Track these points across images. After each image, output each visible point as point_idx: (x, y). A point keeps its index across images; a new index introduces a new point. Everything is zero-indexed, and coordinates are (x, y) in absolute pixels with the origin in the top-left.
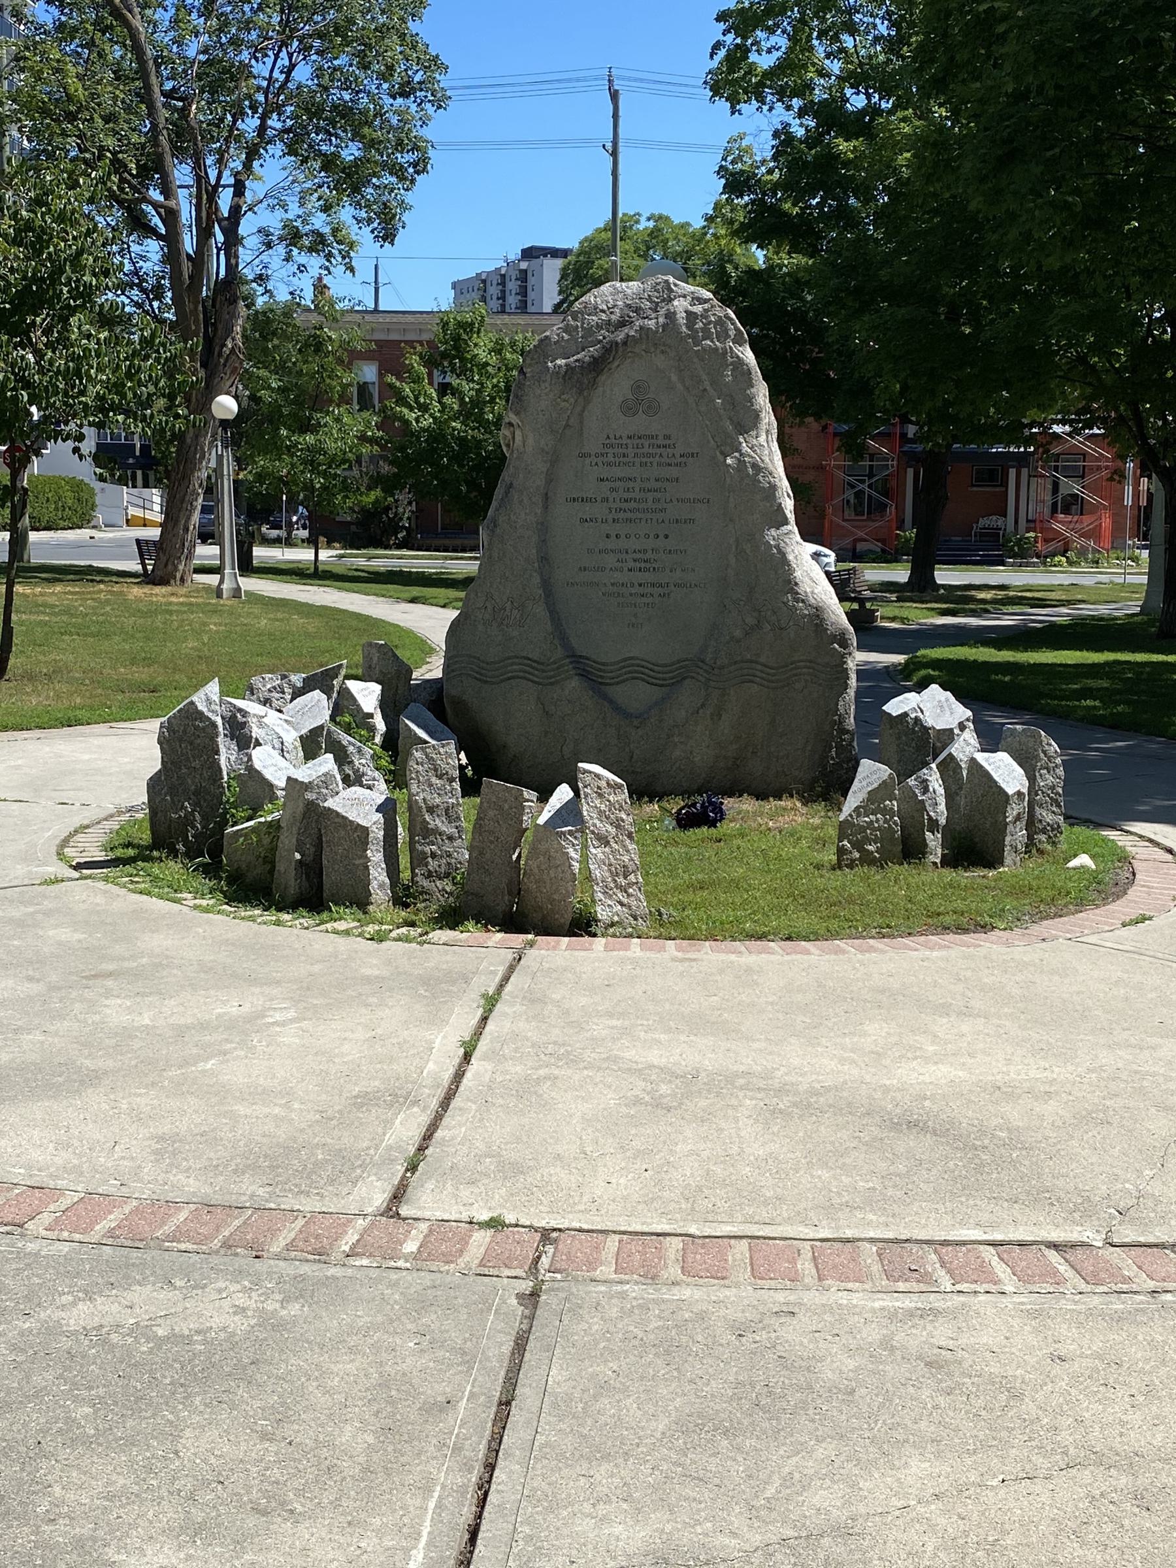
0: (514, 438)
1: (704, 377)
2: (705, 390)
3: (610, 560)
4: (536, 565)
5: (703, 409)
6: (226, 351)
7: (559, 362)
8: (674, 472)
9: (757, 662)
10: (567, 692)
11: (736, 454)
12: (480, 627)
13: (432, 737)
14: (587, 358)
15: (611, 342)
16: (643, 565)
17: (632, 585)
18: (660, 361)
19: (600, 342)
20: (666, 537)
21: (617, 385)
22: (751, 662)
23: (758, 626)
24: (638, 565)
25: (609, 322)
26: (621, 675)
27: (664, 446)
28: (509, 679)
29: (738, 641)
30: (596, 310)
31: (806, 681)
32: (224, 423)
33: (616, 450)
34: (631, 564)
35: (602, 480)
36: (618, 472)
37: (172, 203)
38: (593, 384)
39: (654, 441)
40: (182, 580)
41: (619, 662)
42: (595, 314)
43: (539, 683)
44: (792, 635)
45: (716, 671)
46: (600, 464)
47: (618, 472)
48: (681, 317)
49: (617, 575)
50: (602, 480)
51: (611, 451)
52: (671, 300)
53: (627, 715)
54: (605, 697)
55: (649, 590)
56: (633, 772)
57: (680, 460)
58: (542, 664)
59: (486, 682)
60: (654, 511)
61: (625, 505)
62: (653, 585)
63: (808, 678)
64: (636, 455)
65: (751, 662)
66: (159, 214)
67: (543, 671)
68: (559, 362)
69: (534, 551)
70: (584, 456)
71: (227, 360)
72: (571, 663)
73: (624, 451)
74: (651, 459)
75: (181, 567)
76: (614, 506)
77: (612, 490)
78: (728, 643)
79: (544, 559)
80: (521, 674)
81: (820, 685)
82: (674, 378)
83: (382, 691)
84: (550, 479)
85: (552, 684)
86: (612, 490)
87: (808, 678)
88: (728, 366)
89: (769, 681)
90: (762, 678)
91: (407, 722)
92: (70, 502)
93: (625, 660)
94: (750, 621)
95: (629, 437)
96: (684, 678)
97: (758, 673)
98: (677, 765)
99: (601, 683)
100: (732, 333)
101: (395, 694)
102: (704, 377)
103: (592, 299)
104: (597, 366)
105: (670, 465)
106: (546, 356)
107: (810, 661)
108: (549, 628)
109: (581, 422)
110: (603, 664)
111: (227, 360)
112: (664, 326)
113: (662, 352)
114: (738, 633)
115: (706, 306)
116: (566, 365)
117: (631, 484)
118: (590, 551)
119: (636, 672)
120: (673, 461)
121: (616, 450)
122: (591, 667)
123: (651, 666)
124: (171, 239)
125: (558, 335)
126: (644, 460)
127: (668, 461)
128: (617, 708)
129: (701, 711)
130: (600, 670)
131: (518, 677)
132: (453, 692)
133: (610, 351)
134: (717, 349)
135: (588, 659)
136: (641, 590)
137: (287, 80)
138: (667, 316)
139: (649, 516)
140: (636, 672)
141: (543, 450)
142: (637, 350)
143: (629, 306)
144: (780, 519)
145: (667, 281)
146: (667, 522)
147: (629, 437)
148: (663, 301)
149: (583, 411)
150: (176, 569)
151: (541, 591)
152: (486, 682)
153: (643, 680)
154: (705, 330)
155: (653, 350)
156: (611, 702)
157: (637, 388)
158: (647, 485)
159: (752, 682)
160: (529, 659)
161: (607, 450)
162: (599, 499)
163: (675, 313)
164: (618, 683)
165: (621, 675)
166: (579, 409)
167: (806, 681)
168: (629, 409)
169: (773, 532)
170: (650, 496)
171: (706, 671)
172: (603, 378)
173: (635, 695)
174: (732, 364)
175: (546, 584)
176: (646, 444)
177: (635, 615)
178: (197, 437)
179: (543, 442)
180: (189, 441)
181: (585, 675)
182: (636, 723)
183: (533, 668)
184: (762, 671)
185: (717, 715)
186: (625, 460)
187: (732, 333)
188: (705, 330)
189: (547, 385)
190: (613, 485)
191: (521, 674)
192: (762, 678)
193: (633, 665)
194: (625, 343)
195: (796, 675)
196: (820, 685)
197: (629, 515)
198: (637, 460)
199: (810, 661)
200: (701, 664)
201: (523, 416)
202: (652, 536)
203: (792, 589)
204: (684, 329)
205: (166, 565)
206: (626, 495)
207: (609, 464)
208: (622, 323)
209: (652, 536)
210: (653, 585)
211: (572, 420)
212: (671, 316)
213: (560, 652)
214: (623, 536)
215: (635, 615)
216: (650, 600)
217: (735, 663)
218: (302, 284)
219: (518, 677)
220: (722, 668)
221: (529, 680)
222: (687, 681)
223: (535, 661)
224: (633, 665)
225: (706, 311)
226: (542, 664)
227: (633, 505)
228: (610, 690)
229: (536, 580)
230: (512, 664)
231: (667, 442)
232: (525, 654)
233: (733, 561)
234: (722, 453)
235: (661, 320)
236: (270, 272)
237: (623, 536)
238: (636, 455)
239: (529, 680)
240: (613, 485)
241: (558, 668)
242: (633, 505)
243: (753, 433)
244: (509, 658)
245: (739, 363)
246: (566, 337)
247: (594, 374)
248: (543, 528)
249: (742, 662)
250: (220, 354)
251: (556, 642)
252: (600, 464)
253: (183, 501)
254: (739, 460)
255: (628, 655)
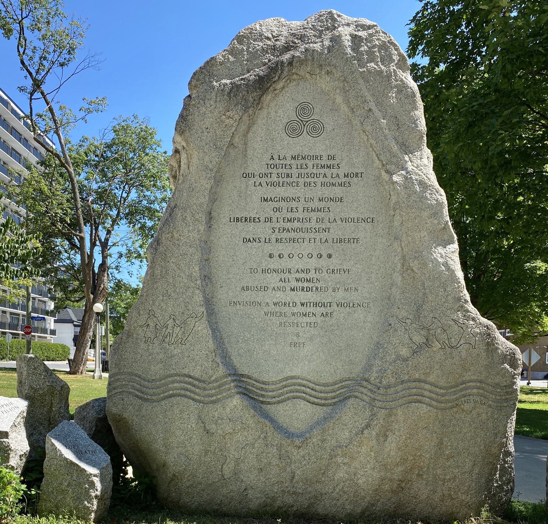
0: (180, 166)
1: (369, 98)
2: (370, 110)
3: (273, 280)
4: (199, 282)
5: (368, 128)
6: (101, 289)
7: (224, 81)
8: (337, 191)
9: (425, 382)
10: (228, 410)
11: (404, 172)
12: (143, 345)
13: (80, 459)
14: (253, 77)
15: (277, 63)
16: (306, 285)
17: (295, 304)
18: (324, 83)
19: (264, 64)
20: (330, 256)
21: (281, 106)
22: (419, 381)
23: (427, 343)
24: (300, 284)
25: (274, 48)
26: (282, 394)
27: (329, 167)
28: (171, 396)
29: (406, 360)
30: (261, 37)
31: (475, 402)
32: (98, 314)
33: (280, 171)
34: (294, 284)
35: (266, 200)
36: (281, 192)
37: (82, 235)
38: (258, 101)
39: (316, 162)
40: (82, 373)
41: (281, 381)
42: (261, 40)
43: (200, 402)
44: (464, 354)
45: (382, 391)
46: (264, 184)
47: (281, 192)
48: (347, 41)
49: (279, 294)
50: (266, 200)
51: (275, 171)
52: (335, 28)
53: (289, 435)
54: (266, 416)
55: (312, 309)
56: (294, 493)
57: (344, 180)
58: (204, 382)
59: (147, 400)
60: (317, 231)
61: (289, 225)
62: (316, 304)
63: (478, 399)
64: (300, 175)
65: (419, 381)
66: (77, 238)
67: (205, 389)
68: (224, 81)
69: (197, 268)
70: (246, 176)
71: (101, 292)
72: (234, 381)
73: (289, 171)
74: (316, 179)
75: (81, 368)
76: (278, 225)
77: (278, 210)
78: (395, 362)
79: (207, 278)
80: (183, 392)
81: (490, 406)
82: (339, 99)
83: (29, 407)
84: (214, 198)
85: (213, 402)
86: (278, 210)
87: (478, 399)
88: (392, 88)
89: (437, 401)
90: (430, 398)
91: (54, 441)
92: (61, 352)
93: (287, 379)
94: (418, 339)
95: (293, 158)
96: (349, 397)
97: (427, 393)
98: (340, 487)
99: (262, 402)
100: (396, 58)
101: (50, 410)
102: (369, 98)
103: (258, 27)
104: (263, 84)
105: (333, 185)
106: (211, 76)
107: (481, 382)
108: (211, 345)
109: (246, 144)
110: (264, 383)
111: (101, 292)
112: (329, 49)
113: (328, 73)
114: (405, 352)
115: (370, 31)
116: (231, 83)
117: (294, 204)
118: (253, 271)
119: (297, 391)
120: (336, 181)
121: (280, 171)
122: (253, 386)
123: (311, 385)
124: (81, 249)
125: (223, 56)
126: (308, 180)
127: (332, 181)
128: (278, 427)
129: (366, 432)
130: (262, 389)
131: (180, 395)
132: (114, 410)
133: (275, 69)
134: (381, 72)
135: (249, 377)
136: (303, 310)
137: (127, 196)
138: (331, 40)
139: (312, 235)
140: (297, 391)
141: (207, 167)
142: (302, 73)
143: (294, 35)
144: (446, 237)
145: (330, 13)
146: (330, 241)
147: (293, 158)
148: (328, 29)
149: (248, 132)
150: (79, 369)
151: (203, 309)
152: (147, 400)
153: (304, 399)
154: (370, 53)
155: (318, 71)
156: (272, 421)
157: (303, 109)
158: (311, 205)
159: (421, 402)
160: (190, 377)
161: (270, 170)
162: (262, 219)
163: (340, 36)
164: (279, 402)
165: (282, 394)
166: (243, 127)
167: (475, 402)
168: (293, 130)
169: (440, 249)
170: (314, 216)
171: (371, 390)
172: (267, 98)
173: (297, 414)
174: (396, 86)
175: (209, 303)
176: (310, 164)
177: (298, 335)
178: (89, 320)
179: (207, 159)
180: (86, 321)
181: (246, 394)
182: (297, 442)
183: (194, 386)
184: (431, 392)
185: (384, 435)
186: (289, 180)
187: (396, 58)
188: (370, 53)
189: (212, 103)
190: (276, 205)
191: (183, 392)
192: (430, 398)
193: (294, 384)
194: (290, 63)
195: (465, 396)
196: (490, 406)
197: (292, 235)
198: (301, 181)
199: (481, 382)
200: (365, 383)
201: (187, 134)
202: (315, 256)
203: (462, 307)
204: (349, 50)
205: (75, 367)
206: (289, 215)
207: (273, 184)
208: (287, 48)
209: (315, 256)
210: (316, 304)
211: (236, 140)
212: (336, 40)
213: (221, 370)
214: (286, 256)
215: (298, 335)
216: (312, 319)
217: (402, 382)
218: (132, 270)
219: (180, 395)
220: (389, 387)
221: (190, 398)
222: (351, 401)
223: (197, 379)
224: (294, 384)
225: (371, 35)
226: (204, 382)
227: (296, 225)
228: (271, 409)
229: (199, 298)
230: (173, 382)
231: (331, 162)
232: (186, 371)
233: (398, 279)
234: (387, 172)
235: (327, 43)
236: (121, 265)
237: (286, 256)
238: (300, 175)
239: (190, 398)
240: (276, 205)
241: (219, 386)
242: (296, 225)
243: (418, 154)
244: (171, 376)
245: (402, 87)
246: (232, 59)
247: (259, 92)
248: (206, 248)
249: (409, 381)
250: (99, 290)
251: (218, 360)
252: (264, 184)
253: (83, 343)
254: (406, 178)
255: (290, 374)
